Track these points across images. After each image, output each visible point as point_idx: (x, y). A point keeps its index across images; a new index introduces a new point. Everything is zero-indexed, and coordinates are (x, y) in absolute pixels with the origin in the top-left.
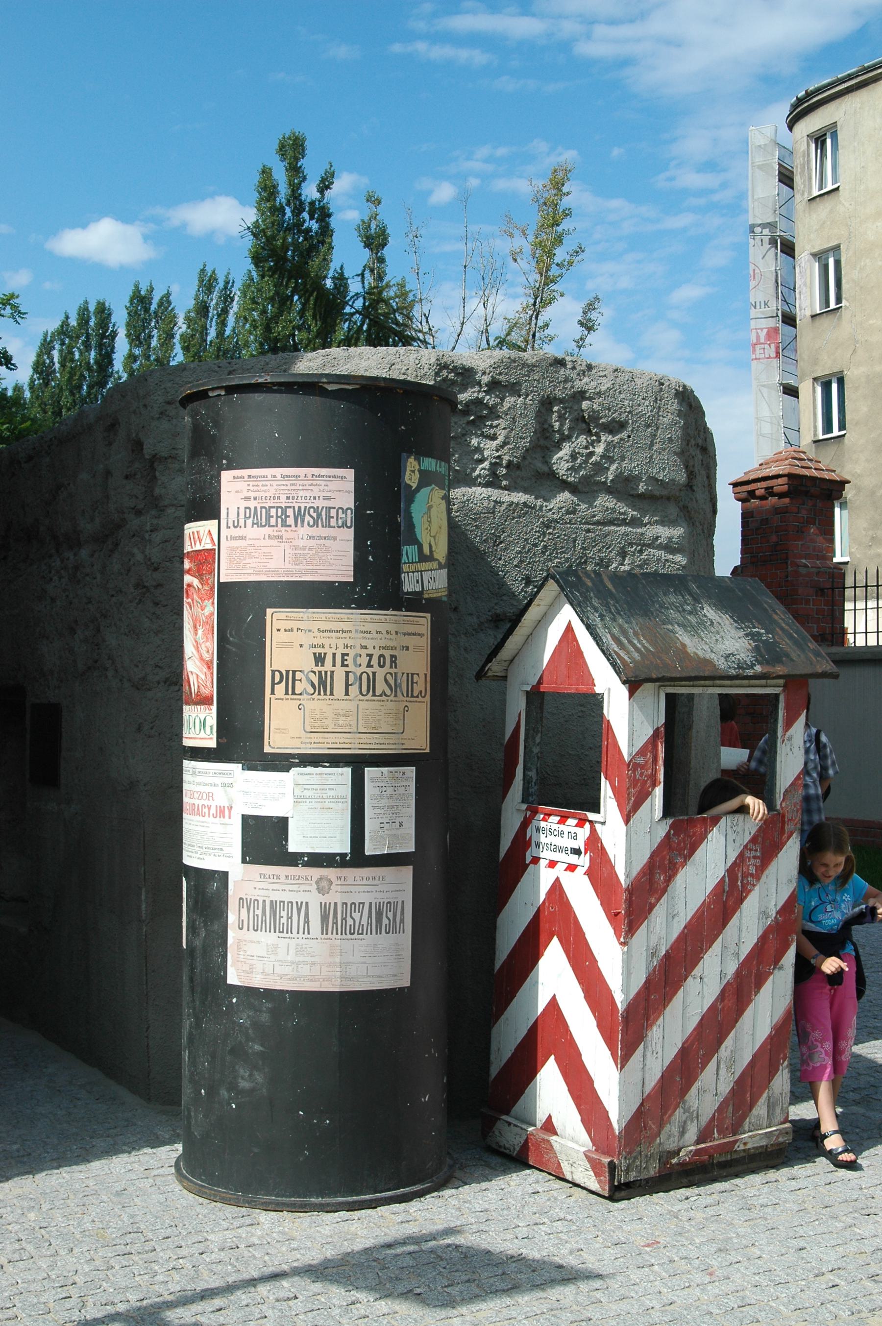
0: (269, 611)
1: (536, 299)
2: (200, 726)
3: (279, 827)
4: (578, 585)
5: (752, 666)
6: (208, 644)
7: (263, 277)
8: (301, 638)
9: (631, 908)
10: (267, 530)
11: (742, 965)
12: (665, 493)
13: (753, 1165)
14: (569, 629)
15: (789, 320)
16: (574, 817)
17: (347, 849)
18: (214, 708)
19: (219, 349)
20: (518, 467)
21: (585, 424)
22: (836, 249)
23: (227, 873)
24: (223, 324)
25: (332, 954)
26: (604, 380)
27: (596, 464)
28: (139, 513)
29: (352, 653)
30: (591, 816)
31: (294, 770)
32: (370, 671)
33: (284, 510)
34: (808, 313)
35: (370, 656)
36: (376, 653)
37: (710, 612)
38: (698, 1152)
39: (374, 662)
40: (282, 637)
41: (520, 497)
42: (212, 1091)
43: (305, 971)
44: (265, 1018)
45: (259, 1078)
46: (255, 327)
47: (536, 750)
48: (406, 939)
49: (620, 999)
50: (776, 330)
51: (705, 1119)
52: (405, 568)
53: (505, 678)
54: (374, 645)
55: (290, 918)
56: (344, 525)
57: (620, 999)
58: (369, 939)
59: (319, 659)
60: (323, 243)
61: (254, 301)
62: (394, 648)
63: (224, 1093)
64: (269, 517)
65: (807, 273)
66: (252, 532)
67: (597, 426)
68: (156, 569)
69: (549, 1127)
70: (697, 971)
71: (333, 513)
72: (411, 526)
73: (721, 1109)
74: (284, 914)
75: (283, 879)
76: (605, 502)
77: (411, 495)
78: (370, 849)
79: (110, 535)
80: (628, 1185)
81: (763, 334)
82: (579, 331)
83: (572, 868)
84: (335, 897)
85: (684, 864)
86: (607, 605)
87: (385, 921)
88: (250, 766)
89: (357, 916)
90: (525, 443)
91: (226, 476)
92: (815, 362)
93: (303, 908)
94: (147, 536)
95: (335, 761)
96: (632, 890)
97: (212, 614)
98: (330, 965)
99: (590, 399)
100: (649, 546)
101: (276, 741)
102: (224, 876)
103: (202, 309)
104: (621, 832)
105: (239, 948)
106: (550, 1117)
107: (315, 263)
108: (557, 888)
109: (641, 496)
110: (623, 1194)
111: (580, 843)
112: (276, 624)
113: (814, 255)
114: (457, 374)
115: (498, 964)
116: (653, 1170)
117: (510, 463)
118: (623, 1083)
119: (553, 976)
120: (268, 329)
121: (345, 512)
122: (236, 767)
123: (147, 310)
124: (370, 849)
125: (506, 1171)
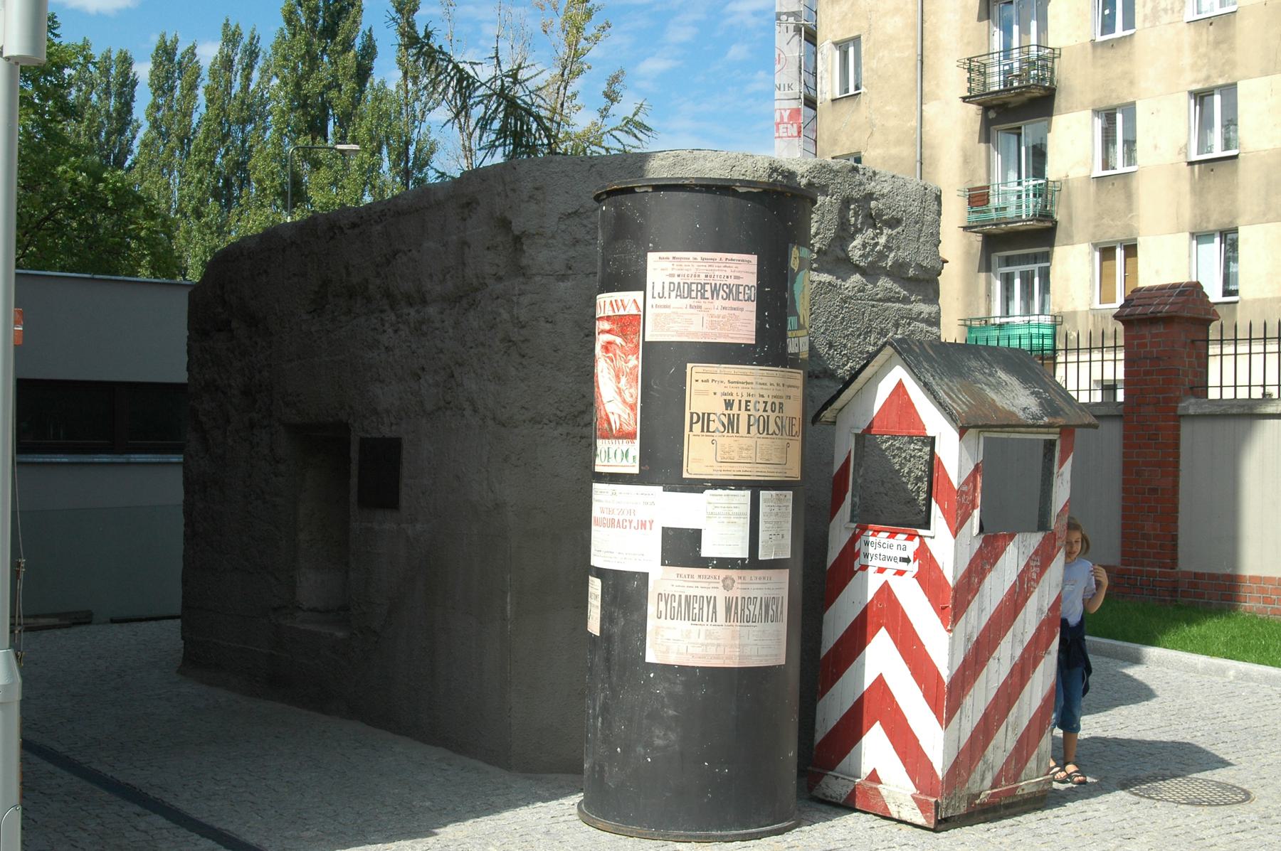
0: (689, 366)
1: (565, 68)
2: (618, 455)
3: (695, 536)
4: (910, 351)
5: (1041, 418)
6: (633, 391)
7: (294, 35)
8: (712, 387)
9: (953, 602)
10: (689, 301)
11: (1025, 650)
12: (927, 277)
13: (1025, 807)
14: (900, 385)
15: (811, 103)
16: (903, 533)
17: (746, 555)
18: (637, 441)
19: (243, 102)
20: (825, 253)
21: (872, 220)
22: (856, 40)
23: (647, 574)
24: (248, 79)
25: (733, 637)
26: (885, 185)
27: (880, 252)
28: (500, 279)
29: (753, 400)
30: (921, 532)
31: (707, 492)
32: (765, 414)
33: (703, 286)
34: (829, 97)
35: (766, 403)
36: (770, 401)
37: (1001, 374)
38: (993, 795)
39: (768, 408)
40: (700, 386)
41: (825, 278)
42: (627, 749)
43: (712, 650)
44: (679, 689)
45: (672, 736)
46: (286, 84)
47: (859, 481)
48: (783, 626)
49: (946, 674)
50: (799, 110)
51: (997, 770)
52: (789, 334)
53: (834, 423)
54: (768, 394)
55: (701, 609)
56: (749, 299)
57: (946, 674)
58: (760, 626)
59: (729, 404)
60: (353, 5)
61: (285, 58)
62: (781, 397)
63: (640, 750)
64: (690, 290)
65: (828, 59)
66: (676, 302)
67: (881, 221)
68: (523, 327)
69: (874, 777)
70: (996, 654)
71: (741, 289)
72: (793, 302)
73: (1007, 762)
74: (696, 606)
75: (696, 578)
76: (884, 282)
77: (795, 275)
78: (762, 556)
79: (465, 297)
80: (945, 820)
81: (786, 114)
82: (604, 102)
83: (900, 573)
84: (736, 592)
85: (990, 570)
86: (933, 367)
87: (771, 612)
88: (670, 487)
89: (752, 608)
90: (831, 234)
91: (652, 257)
92: (835, 142)
93: (712, 601)
94: (515, 299)
95: (739, 485)
96: (957, 589)
97: (636, 366)
98: (732, 646)
99: (877, 199)
100: (915, 319)
101: (692, 469)
102: (645, 576)
103: (227, 63)
104: (946, 545)
105: (657, 633)
106: (874, 771)
107: (345, 25)
108: (886, 590)
109: (910, 279)
110: (942, 826)
111: (910, 553)
112: (695, 376)
113: (836, 44)
114: (784, 177)
115: (824, 652)
116: (963, 809)
117: (820, 249)
118: (947, 739)
119: (880, 658)
120: (298, 86)
121: (750, 289)
122: (658, 489)
123: (171, 60)
124: (762, 556)
125: (838, 815)
